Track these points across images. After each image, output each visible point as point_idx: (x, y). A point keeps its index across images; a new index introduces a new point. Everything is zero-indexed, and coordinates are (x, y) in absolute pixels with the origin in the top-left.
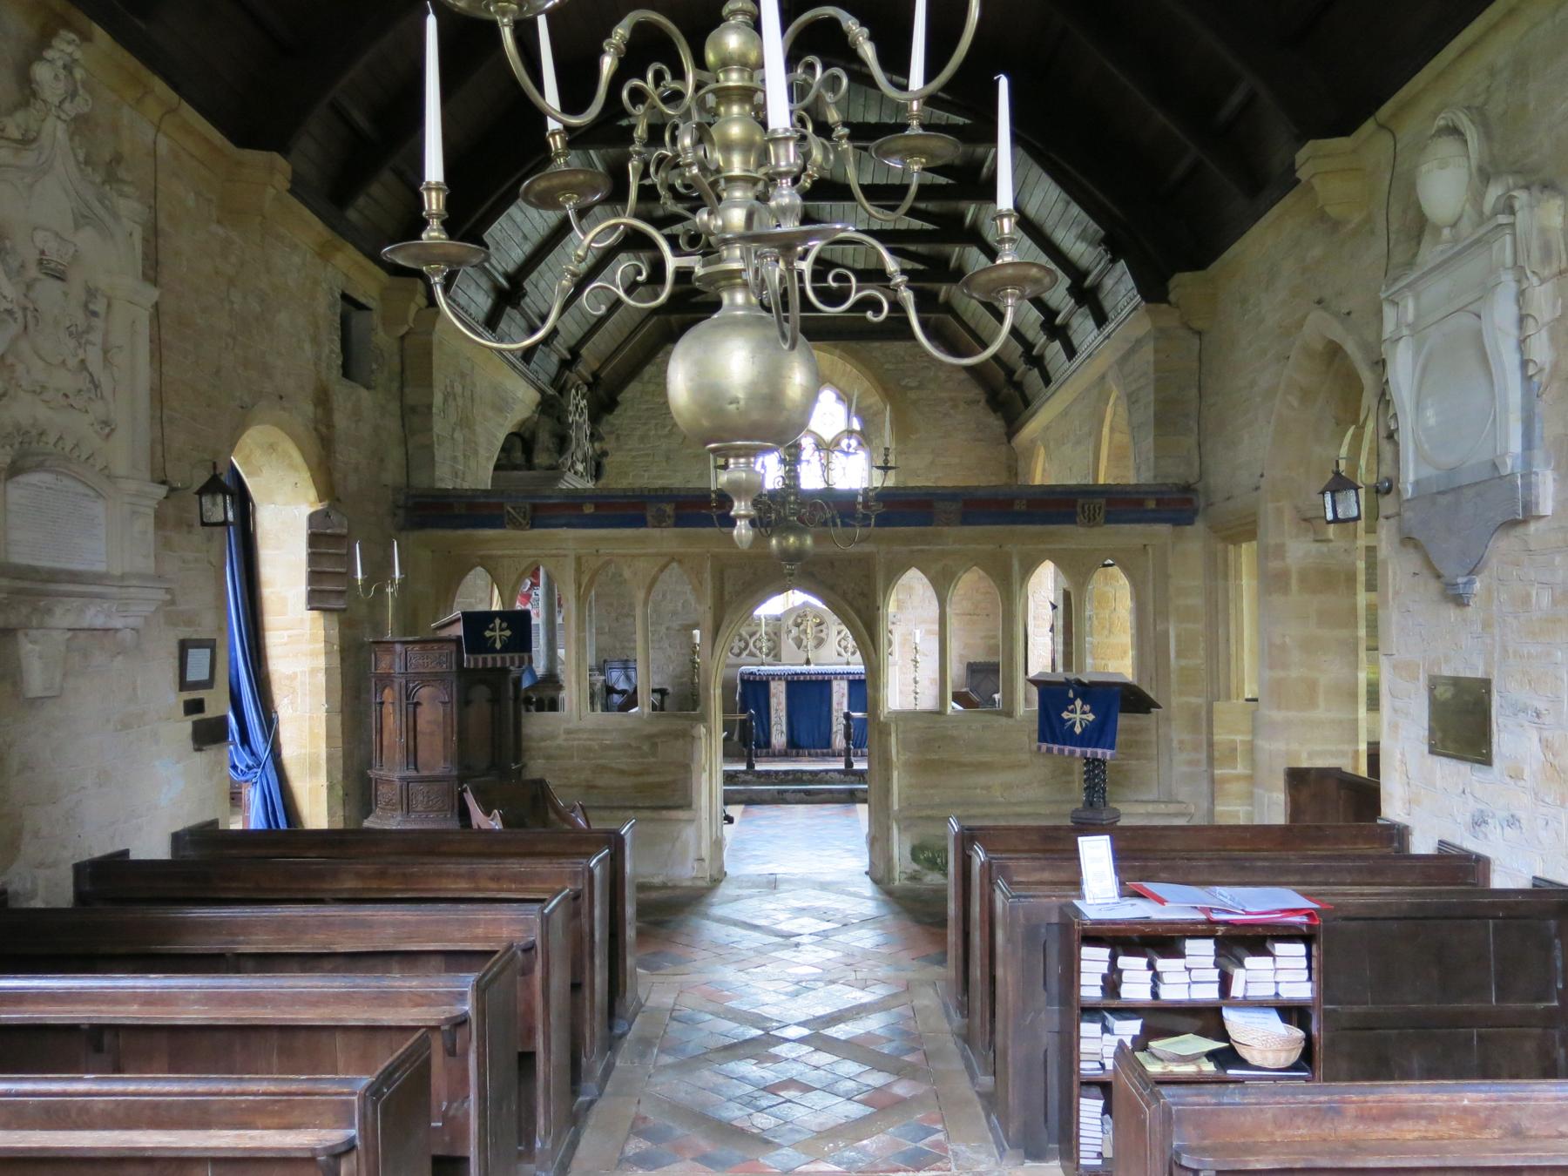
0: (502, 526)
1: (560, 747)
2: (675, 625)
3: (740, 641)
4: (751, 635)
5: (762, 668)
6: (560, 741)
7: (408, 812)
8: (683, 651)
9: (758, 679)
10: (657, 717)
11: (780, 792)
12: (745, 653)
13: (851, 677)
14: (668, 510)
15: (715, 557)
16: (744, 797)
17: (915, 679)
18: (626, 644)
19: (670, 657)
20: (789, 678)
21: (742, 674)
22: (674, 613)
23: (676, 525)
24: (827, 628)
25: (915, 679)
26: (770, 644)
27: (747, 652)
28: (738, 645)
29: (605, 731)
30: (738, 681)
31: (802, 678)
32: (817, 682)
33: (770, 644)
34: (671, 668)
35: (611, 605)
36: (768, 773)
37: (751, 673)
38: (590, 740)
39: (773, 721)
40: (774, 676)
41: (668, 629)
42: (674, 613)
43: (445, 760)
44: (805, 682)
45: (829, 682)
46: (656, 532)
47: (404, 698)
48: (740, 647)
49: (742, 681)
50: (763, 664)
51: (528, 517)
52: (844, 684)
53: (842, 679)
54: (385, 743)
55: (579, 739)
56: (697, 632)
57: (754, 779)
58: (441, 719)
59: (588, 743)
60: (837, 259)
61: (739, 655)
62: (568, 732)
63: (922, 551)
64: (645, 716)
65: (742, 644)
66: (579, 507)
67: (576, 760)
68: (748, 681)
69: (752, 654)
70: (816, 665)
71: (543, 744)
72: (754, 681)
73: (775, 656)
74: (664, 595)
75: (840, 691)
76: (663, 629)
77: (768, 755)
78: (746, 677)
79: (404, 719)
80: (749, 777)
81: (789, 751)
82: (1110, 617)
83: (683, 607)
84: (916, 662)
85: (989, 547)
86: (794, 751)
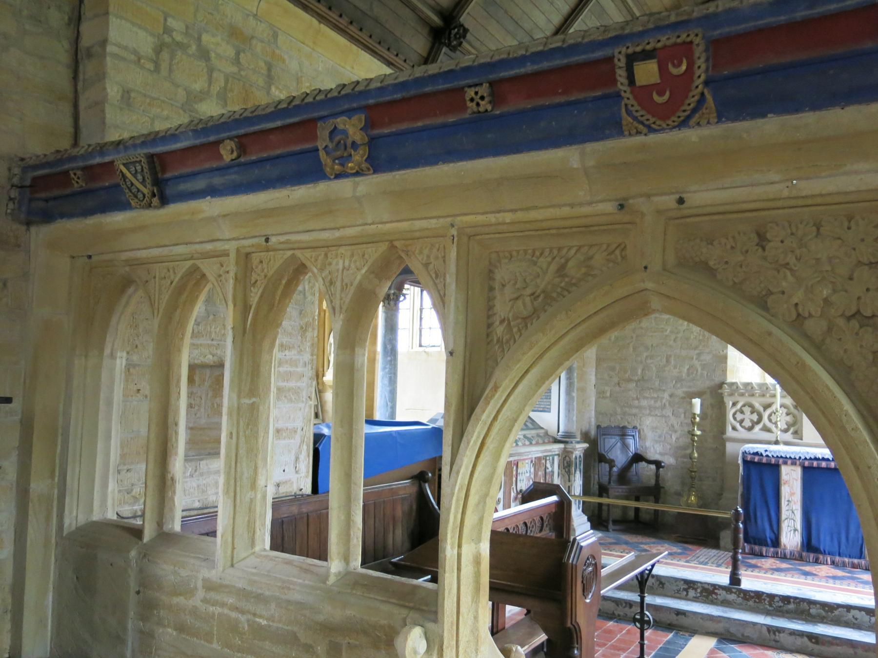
1: (194, 612)
2: (680, 392)
3: (752, 413)
4: (766, 407)
5: (773, 448)
6: (196, 601)
8: (686, 421)
9: (764, 460)
11: (772, 630)
12: (757, 428)
14: (351, 131)
16: (719, 627)
18: (627, 409)
19: (673, 426)
20: (807, 463)
21: (744, 453)
22: (679, 380)
26: (789, 419)
27: (760, 426)
28: (749, 417)
29: (260, 598)
30: (740, 461)
33: (789, 419)
34: (674, 438)
35: (613, 369)
36: (758, 595)
37: (757, 454)
39: (784, 515)
40: (786, 460)
41: (671, 396)
42: (679, 380)
46: (344, 187)
48: (752, 421)
49: (745, 462)
50: (777, 443)
55: (223, 605)
56: (697, 402)
57: (740, 600)
59: (234, 615)
61: (750, 429)
62: (210, 586)
64: (332, 580)
65: (755, 417)
67: (215, 645)
68: (752, 462)
69: (766, 429)
71: (176, 600)
72: (759, 464)
73: (796, 433)
74: (668, 361)
76: (666, 395)
77: (775, 556)
78: (749, 458)
80: (732, 597)
81: (804, 554)
83: (688, 374)
86: (812, 555)
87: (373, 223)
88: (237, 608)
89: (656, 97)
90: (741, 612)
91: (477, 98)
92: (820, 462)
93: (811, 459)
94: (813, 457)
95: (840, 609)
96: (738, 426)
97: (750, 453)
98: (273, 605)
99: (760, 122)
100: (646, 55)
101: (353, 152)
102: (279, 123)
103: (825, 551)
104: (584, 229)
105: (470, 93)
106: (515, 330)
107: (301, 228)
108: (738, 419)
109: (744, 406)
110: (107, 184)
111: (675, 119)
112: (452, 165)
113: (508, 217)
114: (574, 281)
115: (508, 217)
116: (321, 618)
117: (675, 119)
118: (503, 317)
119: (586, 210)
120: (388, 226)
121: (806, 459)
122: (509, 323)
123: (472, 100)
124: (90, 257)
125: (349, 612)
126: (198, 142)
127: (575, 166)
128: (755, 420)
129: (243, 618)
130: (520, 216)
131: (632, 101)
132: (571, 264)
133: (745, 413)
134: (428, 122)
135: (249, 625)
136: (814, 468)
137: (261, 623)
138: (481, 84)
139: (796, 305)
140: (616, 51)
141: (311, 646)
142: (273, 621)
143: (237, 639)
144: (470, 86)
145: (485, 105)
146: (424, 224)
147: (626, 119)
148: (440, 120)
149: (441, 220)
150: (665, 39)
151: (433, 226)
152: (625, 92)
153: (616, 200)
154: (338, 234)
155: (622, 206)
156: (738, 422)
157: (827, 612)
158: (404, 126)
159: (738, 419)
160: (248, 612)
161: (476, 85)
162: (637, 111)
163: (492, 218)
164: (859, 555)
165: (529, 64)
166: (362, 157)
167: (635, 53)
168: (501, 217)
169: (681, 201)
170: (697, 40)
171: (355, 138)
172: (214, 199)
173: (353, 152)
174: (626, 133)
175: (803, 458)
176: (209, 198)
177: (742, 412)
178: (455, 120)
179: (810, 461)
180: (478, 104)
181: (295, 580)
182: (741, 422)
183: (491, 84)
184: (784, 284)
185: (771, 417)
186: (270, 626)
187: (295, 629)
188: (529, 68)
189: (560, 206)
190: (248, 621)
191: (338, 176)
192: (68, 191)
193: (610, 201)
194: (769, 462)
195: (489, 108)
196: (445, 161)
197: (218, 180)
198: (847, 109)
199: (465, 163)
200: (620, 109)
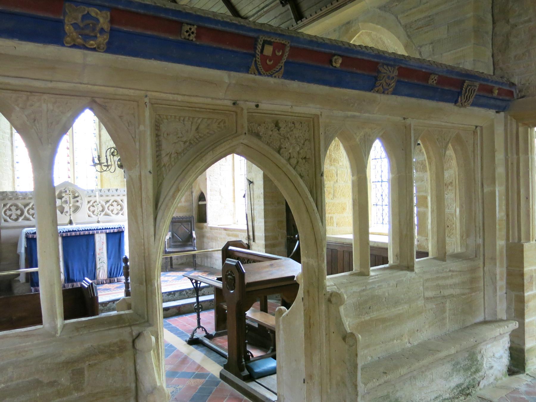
4: (26, 205)
10: (77, 328)
12: (21, 219)
13: (108, 231)
14: (101, 20)
15: (154, 104)
20: (64, 235)
23: (110, 48)
27: (23, 217)
31: (73, 234)
32: (84, 235)
45: (93, 235)
46: (77, 55)
48: (17, 215)
52: (104, 236)
61: (16, 220)
63: (354, 117)
65: (19, 212)
70: (77, 224)
75: (101, 241)
82: (334, 186)
85: (398, 119)
87: (88, 84)
89: (268, 61)
90: (382, 243)
92: (71, 233)
93: (66, 232)
94: (67, 231)
95: (110, 304)
96: (8, 219)
97: (31, 234)
99: (293, 82)
100: (270, 43)
101: (98, 35)
103: (77, 280)
104: (212, 111)
105: (186, 27)
106: (173, 159)
108: (8, 214)
109: (11, 206)
111: (270, 73)
112: (159, 62)
113: (180, 98)
114: (202, 136)
115: (180, 98)
116: (63, 358)
117: (270, 73)
118: (168, 152)
119: (219, 102)
120: (96, 88)
121: (63, 232)
122: (170, 156)
125: (87, 345)
127: (226, 81)
128: (19, 214)
130: (186, 98)
131: (259, 60)
132: (202, 127)
133: (13, 210)
134: (155, 34)
136: (82, 235)
138: (194, 25)
139: (290, 153)
140: (261, 37)
141: (55, 382)
144: (188, 24)
145: (192, 37)
146: (126, 92)
147: (253, 67)
148: (163, 35)
149: (138, 92)
150: (278, 40)
151: (132, 94)
152: (258, 55)
153: (232, 100)
154: (50, 85)
155: (234, 104)
156: (8, 216)
157: (104, 307)
158: (139, 30)
159: (8, 214)
161: (190, 24)
162: (259, 65)
163: (170, 97)
164: (93, 278)
165: (220, 25)
166: (104, 40)
167: (267, 40)
168: (176, 97)
169: (257, 106)
170: (264, 38)
171: (104, 26)
173: (98, 35)
174: (250, 72)
175: (62, 232)
177: (10, 210)
178: (173, 38)
179: (66, 233)
181: (24, 344)
182: (10, 216)
183: (199, 27)
184: (287, 145)
185: (29, 212)
188: (219, 27)
189: (207, 97)
191: (74, 46)
193: (230, 100)
194: (67, 235)
195: (194, 39)
196: (156, 59)
198: (315, 85)
199: (167, 63)
200: (252, 62)
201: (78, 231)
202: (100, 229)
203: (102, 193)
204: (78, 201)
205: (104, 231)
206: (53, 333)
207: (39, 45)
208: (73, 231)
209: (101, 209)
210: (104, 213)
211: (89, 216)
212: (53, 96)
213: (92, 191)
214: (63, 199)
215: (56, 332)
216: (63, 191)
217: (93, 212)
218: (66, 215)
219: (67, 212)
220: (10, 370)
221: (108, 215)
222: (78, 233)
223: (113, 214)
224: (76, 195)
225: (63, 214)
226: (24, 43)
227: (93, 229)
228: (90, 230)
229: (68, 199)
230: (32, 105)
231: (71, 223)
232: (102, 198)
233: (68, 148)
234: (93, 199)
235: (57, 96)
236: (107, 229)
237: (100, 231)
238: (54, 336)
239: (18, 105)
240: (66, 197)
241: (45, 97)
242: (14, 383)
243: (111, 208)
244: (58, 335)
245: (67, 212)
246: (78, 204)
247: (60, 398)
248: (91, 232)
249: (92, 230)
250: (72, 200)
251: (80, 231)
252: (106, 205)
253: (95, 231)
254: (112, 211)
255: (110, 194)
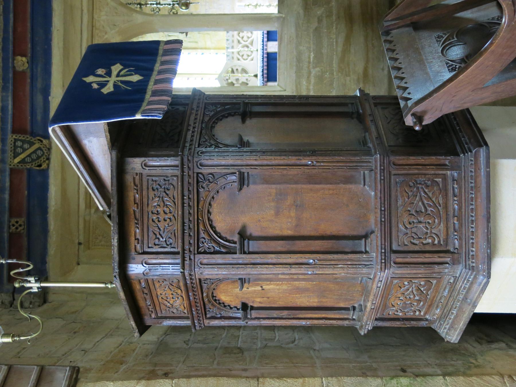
0: (45, 174)
7: (447, 252)
13: (265, 40)
17: (267, 6)
20: (265, 80)
24: (235, 66)
25: (267, 6)
31: (265, 72)
32: (268, 62)
38: (308, 77)
43: (349, 180)
44: (268, 70)
45: (268, 54)
47: (229, 258)
51: (29, 138)
53: (266, 46)
54: (314, 302)
58: (273, 189)
59: (313, 81)
60: (188, 274)
66: (18, 76)
79: (272, 258)
84: (257, 5)
88: (308, 77)
91: (17, 225)
92: (264, 73)
93: (263, 78)
94: (262, 77)
98: (301, 48)
102: (11, 16)
107: (79, 36)
110: (26, 192)
116: (301, 12)
121: (263, 80)
123: (17, 228)
124: (80, 244)
126: (11, 87)
129: (313, 72)
135: (316, 67)
137: (313, 57)
141: (318, 18)
142: (310, 48)
143: (326, 76)
160: (308, 67)
172: (52, 94)
175: (262, 82)
176: (50, 98)
180: (20, 225)
186: (314, 50)
187: (311, 30)
190: (314, 68)
192: (29, 74)
197: (39, 84)
201: (263, 67)
202: (263, 47)
203: (230, 46)
204: (237, 70)
205: (265, 43)
206: (282, 19)
207: (53, 14)
208: (263, 72)
209: (246, 49)
210: (250, 46)
211: (252, 60)
212: (95, 10)
213: (227, 56)
214: (234, 82)
215: (282, 17)
216: (226, 82)
217: (248, 56)
218: (249, 81)
219: (247, 80)
220: (301, 48)
221: (252, 42)
222: (265, 67)
223: (251, 37)
224: (230, 69)
225: (248, 83)
226: (53, 24)
227: (262, 53)
228: (263, 56)
229: (235, 78)
230: (103, 27)
231: (256, 76)
232: (235, 46)
233: (188, 79)
234: (236, 56)
235: (95, 8)
236: (263, 40)
237: (265, 47)
238: (284, 18)
239: (104, 36)
240: (232, 80)
241: (95, 16)
242: (312, 46)
243: (245, 38)
244: (284, 16)
245: (247, 80)
246: (240, 69)
247: (332, 15)
248: (265, 55)
249: (263, 54)
250: (236, 74)
251: (263, 65)
252: (241, 43)
253: (265, 52)
254: (248, 38)
255: (231, 39)
